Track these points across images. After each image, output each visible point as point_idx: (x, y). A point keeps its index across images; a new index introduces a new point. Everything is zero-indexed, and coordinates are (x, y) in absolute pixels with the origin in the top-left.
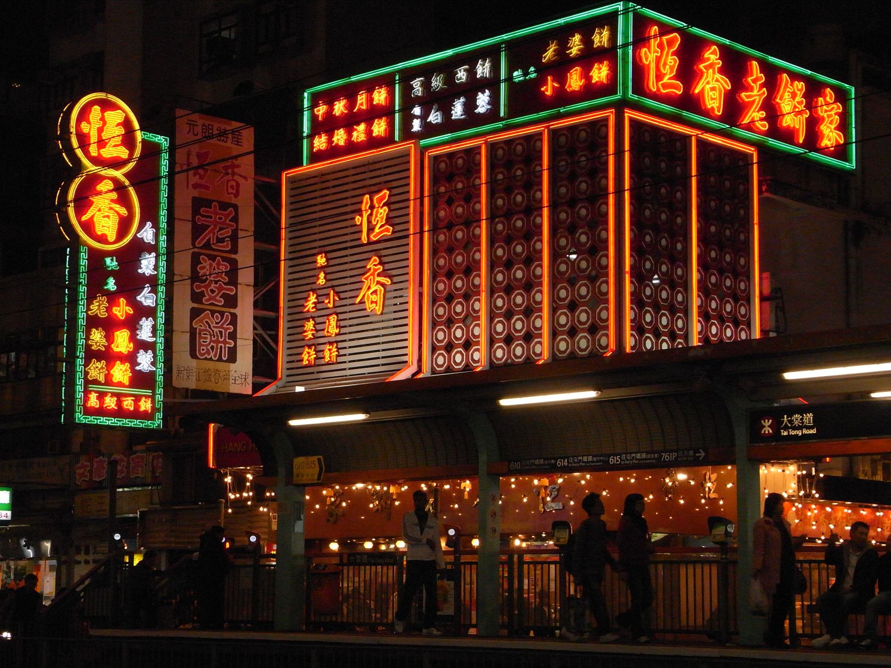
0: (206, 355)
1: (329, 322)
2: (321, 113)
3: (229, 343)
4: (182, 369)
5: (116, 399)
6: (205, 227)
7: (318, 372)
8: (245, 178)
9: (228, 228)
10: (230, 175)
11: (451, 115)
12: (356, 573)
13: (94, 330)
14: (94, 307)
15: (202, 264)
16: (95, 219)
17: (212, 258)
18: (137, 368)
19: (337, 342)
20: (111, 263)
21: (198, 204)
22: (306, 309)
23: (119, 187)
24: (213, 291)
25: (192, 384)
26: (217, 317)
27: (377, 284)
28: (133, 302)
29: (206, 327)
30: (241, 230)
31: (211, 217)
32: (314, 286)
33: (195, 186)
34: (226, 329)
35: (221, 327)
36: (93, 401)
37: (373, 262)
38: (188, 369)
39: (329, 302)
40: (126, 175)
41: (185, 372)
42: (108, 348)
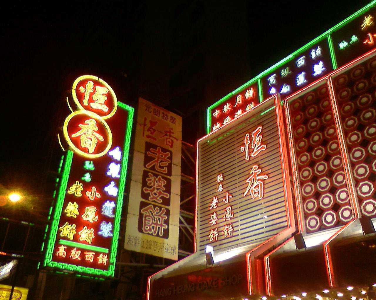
0: (149, 231)
1: (226, 212)
2: (216, 115)
3: (164, 226)
4: (132, 238)
5: (80, 252)
6: (151, 159)
7: (220, 245)
8: (177, 140)
9: (166, 162)
10: (168, 136)
11: (297, 84)
12: (156, 197)
13: (70, 203)
14: (72, 190)
15: (149, 177)
16: (81, 138)
17: (156, 176)
18: (100, 233)
19: (232, 223)
20: (89, 166)
21: (148, 146)
22: (211, 208)
23: (99, 124)
24: (155, 194)
25: (138, 249)
26: (157, 210)
27: (258, 180)
28: (101, 189)
29: (150, 214)
30: (174, 164)
31: (156, 154)
32: (216, 194)
33: (148, 137)
34: (162, 218)
35: (160, 215)
36: (62, 252)
37: (254, 168)
38: (136, 239)
39: (226, 200)
40: (107, 121)
41: (134, 240)
42: (79, 217)
